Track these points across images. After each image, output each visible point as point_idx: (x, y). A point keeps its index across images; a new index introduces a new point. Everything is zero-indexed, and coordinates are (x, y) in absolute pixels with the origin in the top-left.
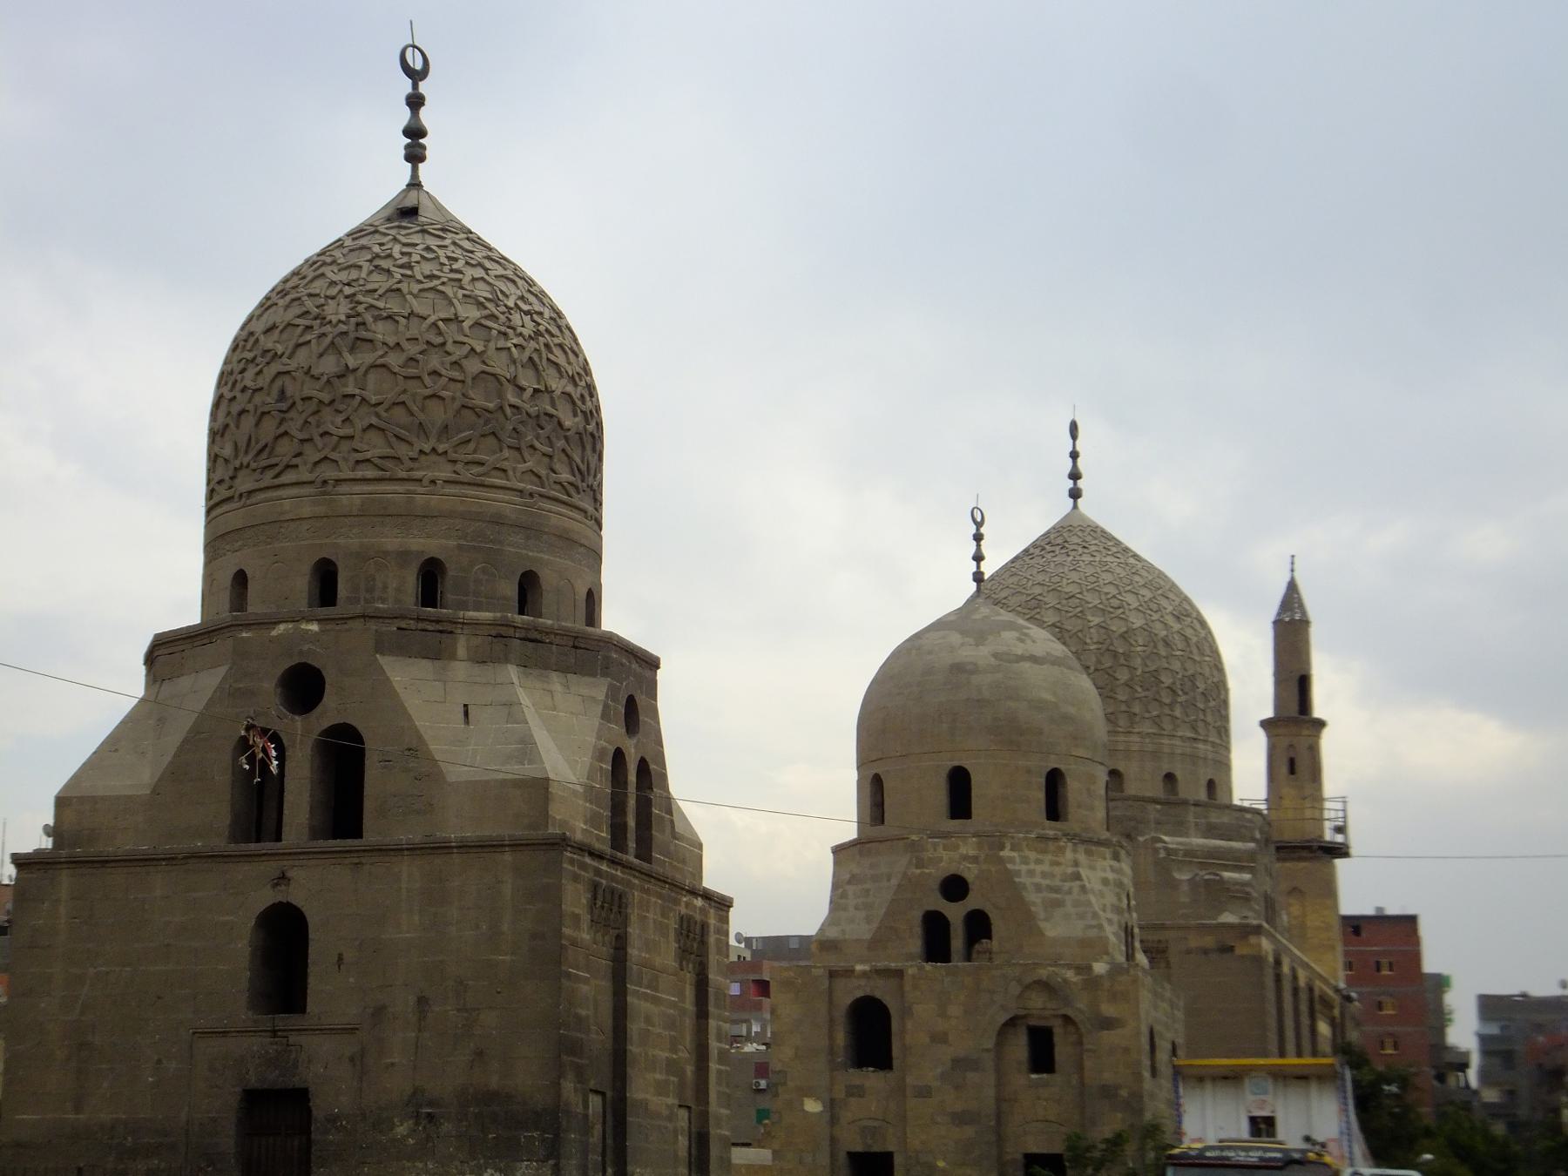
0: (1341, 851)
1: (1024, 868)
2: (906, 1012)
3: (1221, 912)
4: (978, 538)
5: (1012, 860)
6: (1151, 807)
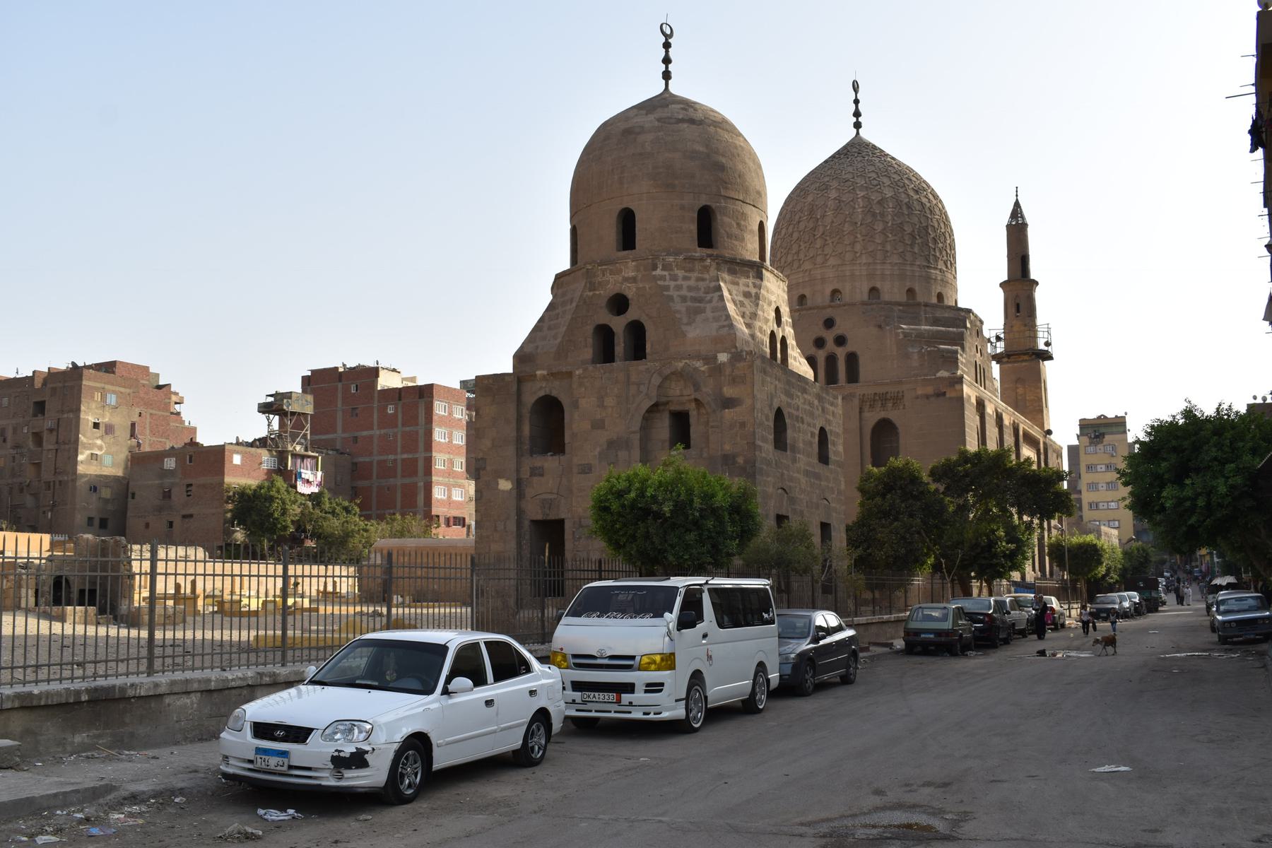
0: (1047, 356)
1: (672, 284)
2: (575, 405)
3: (938, 371)
4: (667, 46)
5: (663, 278)
6: (896, 308)
